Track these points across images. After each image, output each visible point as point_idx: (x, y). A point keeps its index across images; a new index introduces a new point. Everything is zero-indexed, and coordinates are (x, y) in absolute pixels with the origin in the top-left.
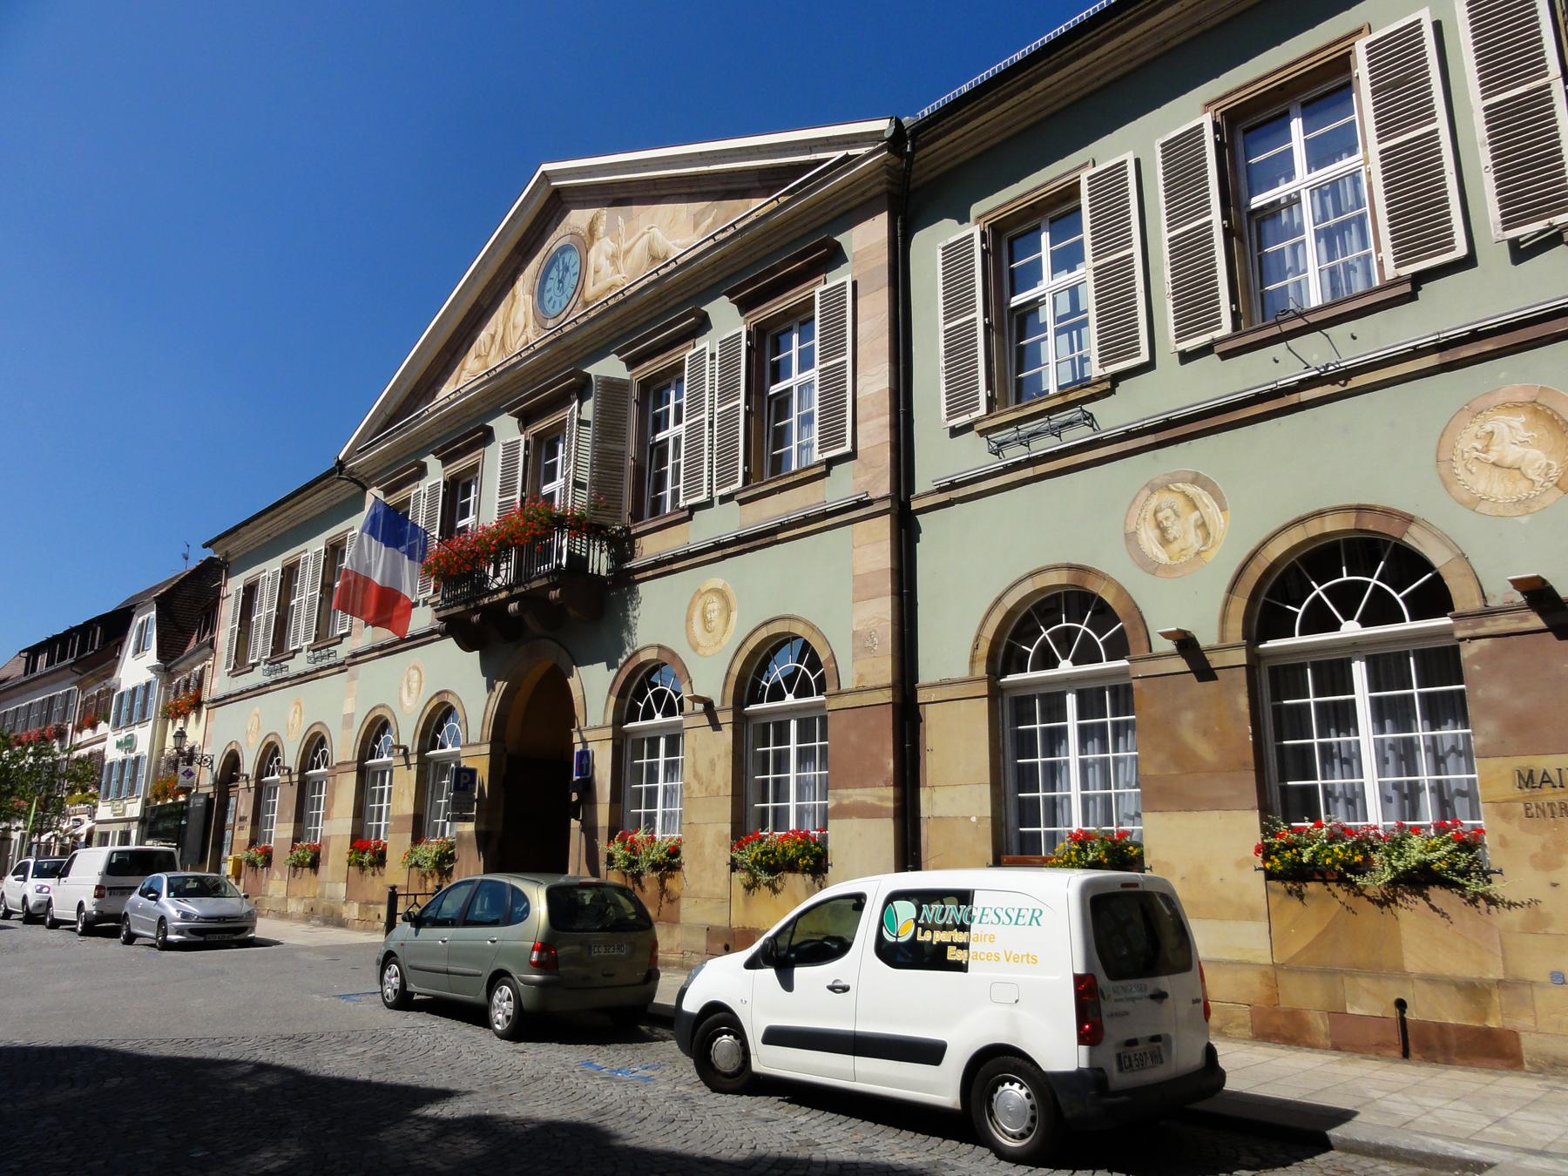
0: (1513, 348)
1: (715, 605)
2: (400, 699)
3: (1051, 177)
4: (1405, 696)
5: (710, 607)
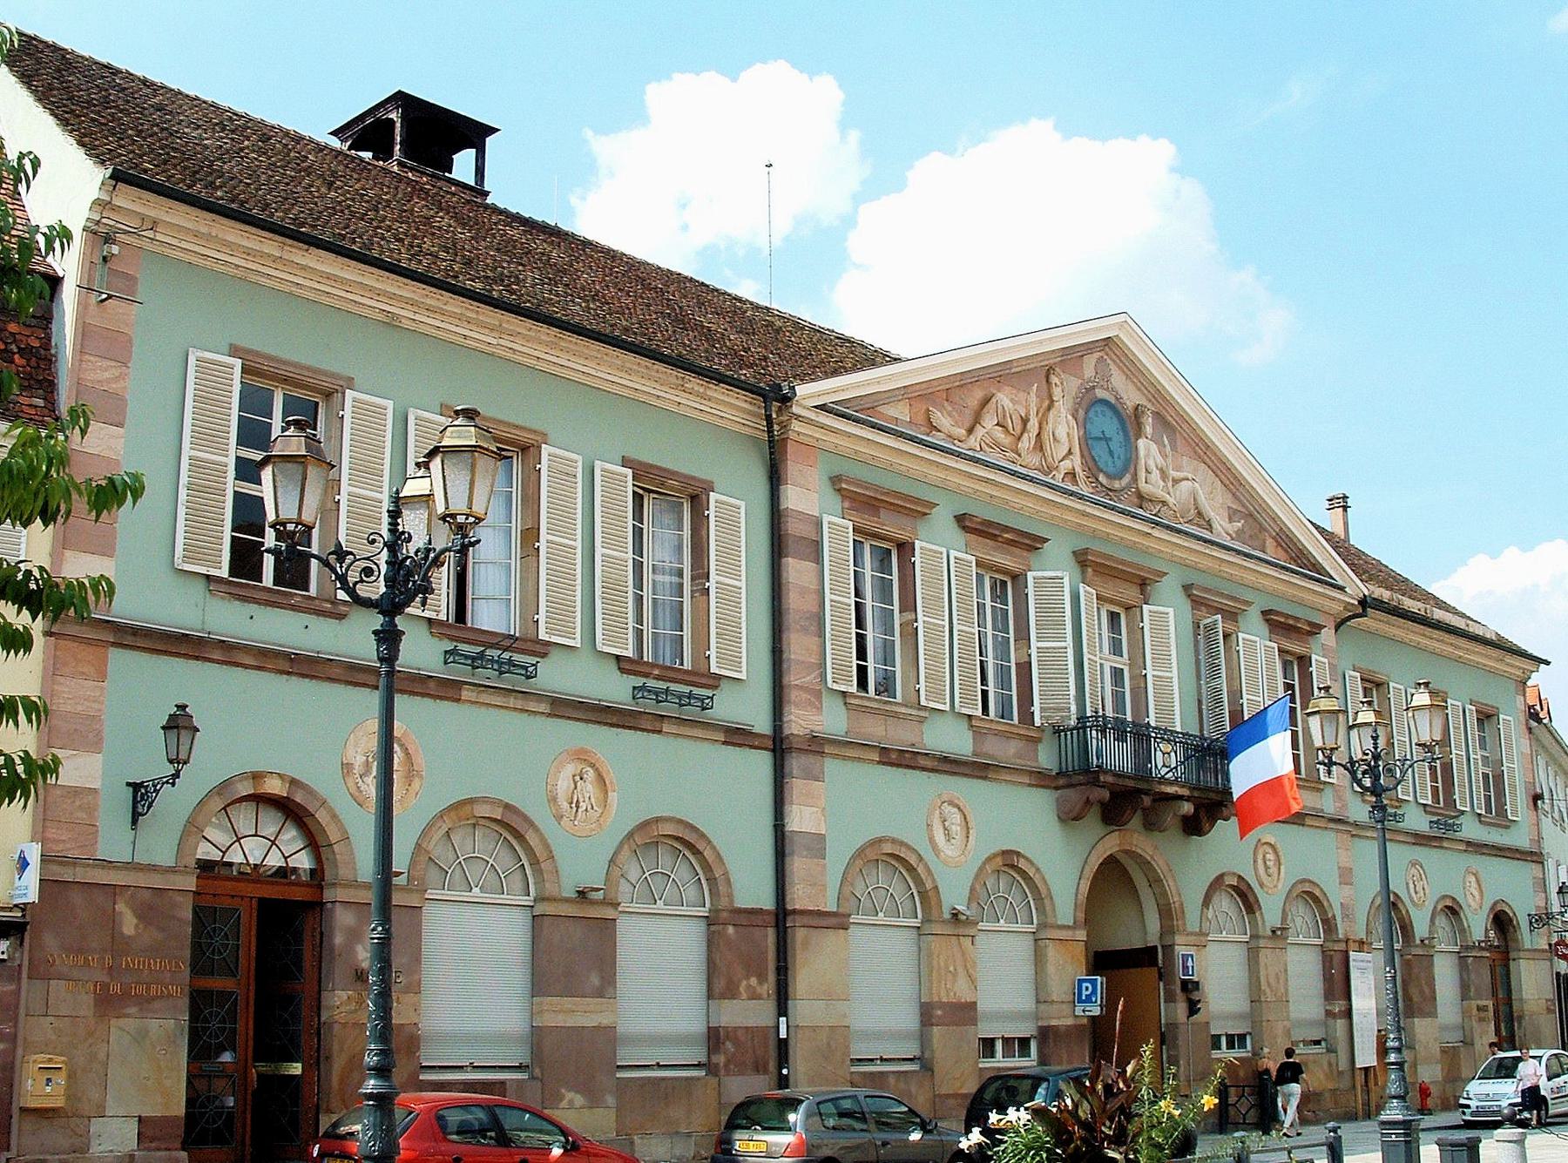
2: (932, 840)
5: (1268, 856)
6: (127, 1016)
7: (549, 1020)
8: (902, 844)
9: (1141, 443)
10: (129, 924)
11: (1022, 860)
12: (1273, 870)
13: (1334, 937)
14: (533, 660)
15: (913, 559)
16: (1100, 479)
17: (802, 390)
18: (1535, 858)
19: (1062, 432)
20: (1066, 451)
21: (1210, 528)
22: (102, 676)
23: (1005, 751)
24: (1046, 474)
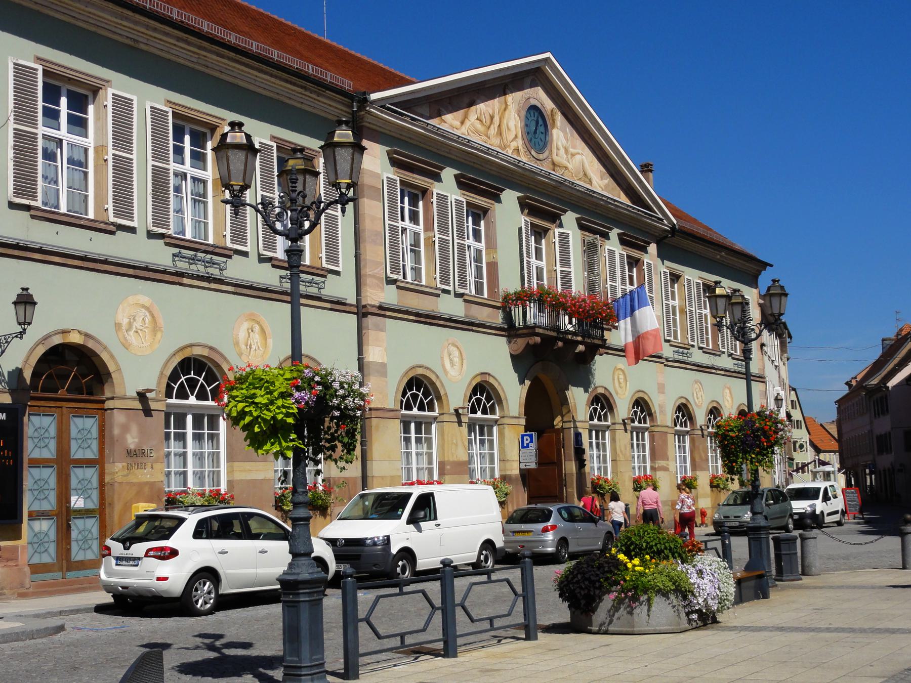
2: (443, 366)
3: (676, 268)
4: (183, 432)
7: (238, 476)
8: (427, 368)
11: (491, 378)
12: (623, 385)
13: (655, 424)
14: (224, 259)
15: (432, 200)
16: (532, 153)
18: (761, 380)
19: (512, 125)
20: (513, 136)
21: (590, 182)
23: (483, 315)
24: (503, 149)
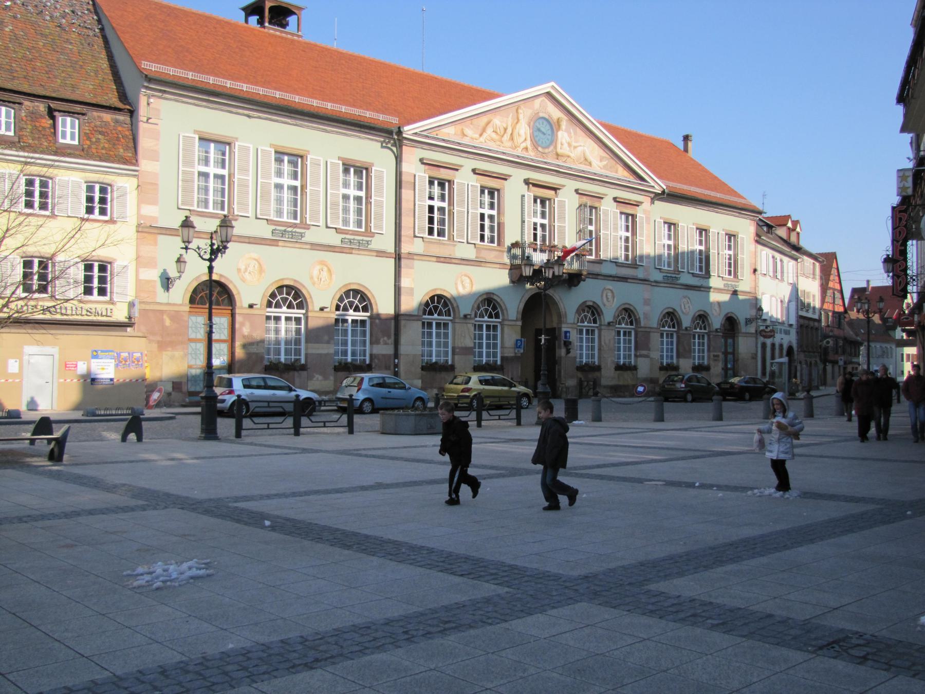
0: (345, 251)
1: (610, 294)
5: (608, 294)
6: (168, 351)
9: (560, 134)
10: (168, 322)
17: (406, 128)
19: (522, 132)
21: (590, 164)
22: (156, 243)
